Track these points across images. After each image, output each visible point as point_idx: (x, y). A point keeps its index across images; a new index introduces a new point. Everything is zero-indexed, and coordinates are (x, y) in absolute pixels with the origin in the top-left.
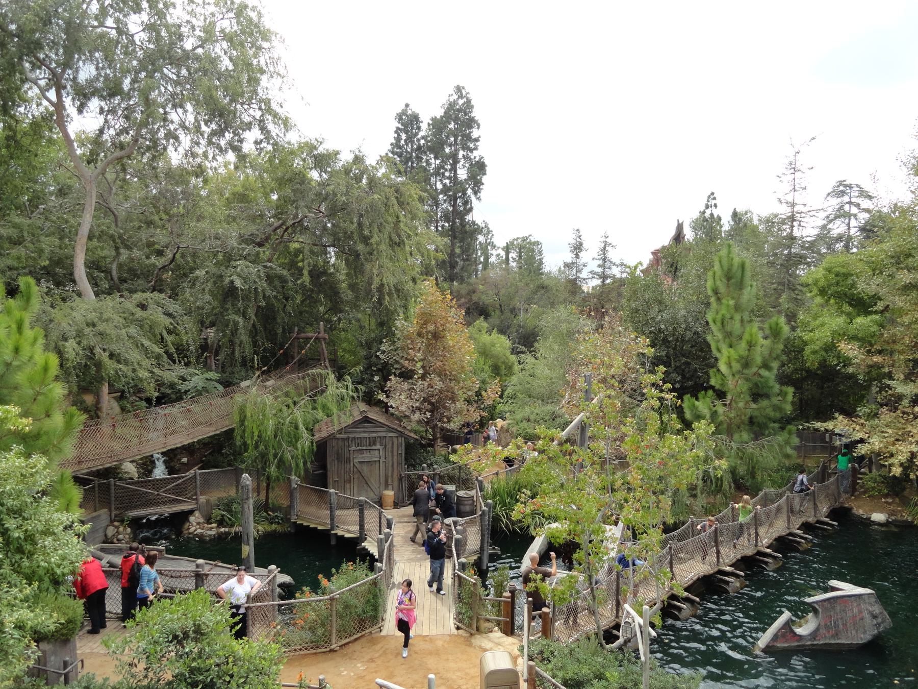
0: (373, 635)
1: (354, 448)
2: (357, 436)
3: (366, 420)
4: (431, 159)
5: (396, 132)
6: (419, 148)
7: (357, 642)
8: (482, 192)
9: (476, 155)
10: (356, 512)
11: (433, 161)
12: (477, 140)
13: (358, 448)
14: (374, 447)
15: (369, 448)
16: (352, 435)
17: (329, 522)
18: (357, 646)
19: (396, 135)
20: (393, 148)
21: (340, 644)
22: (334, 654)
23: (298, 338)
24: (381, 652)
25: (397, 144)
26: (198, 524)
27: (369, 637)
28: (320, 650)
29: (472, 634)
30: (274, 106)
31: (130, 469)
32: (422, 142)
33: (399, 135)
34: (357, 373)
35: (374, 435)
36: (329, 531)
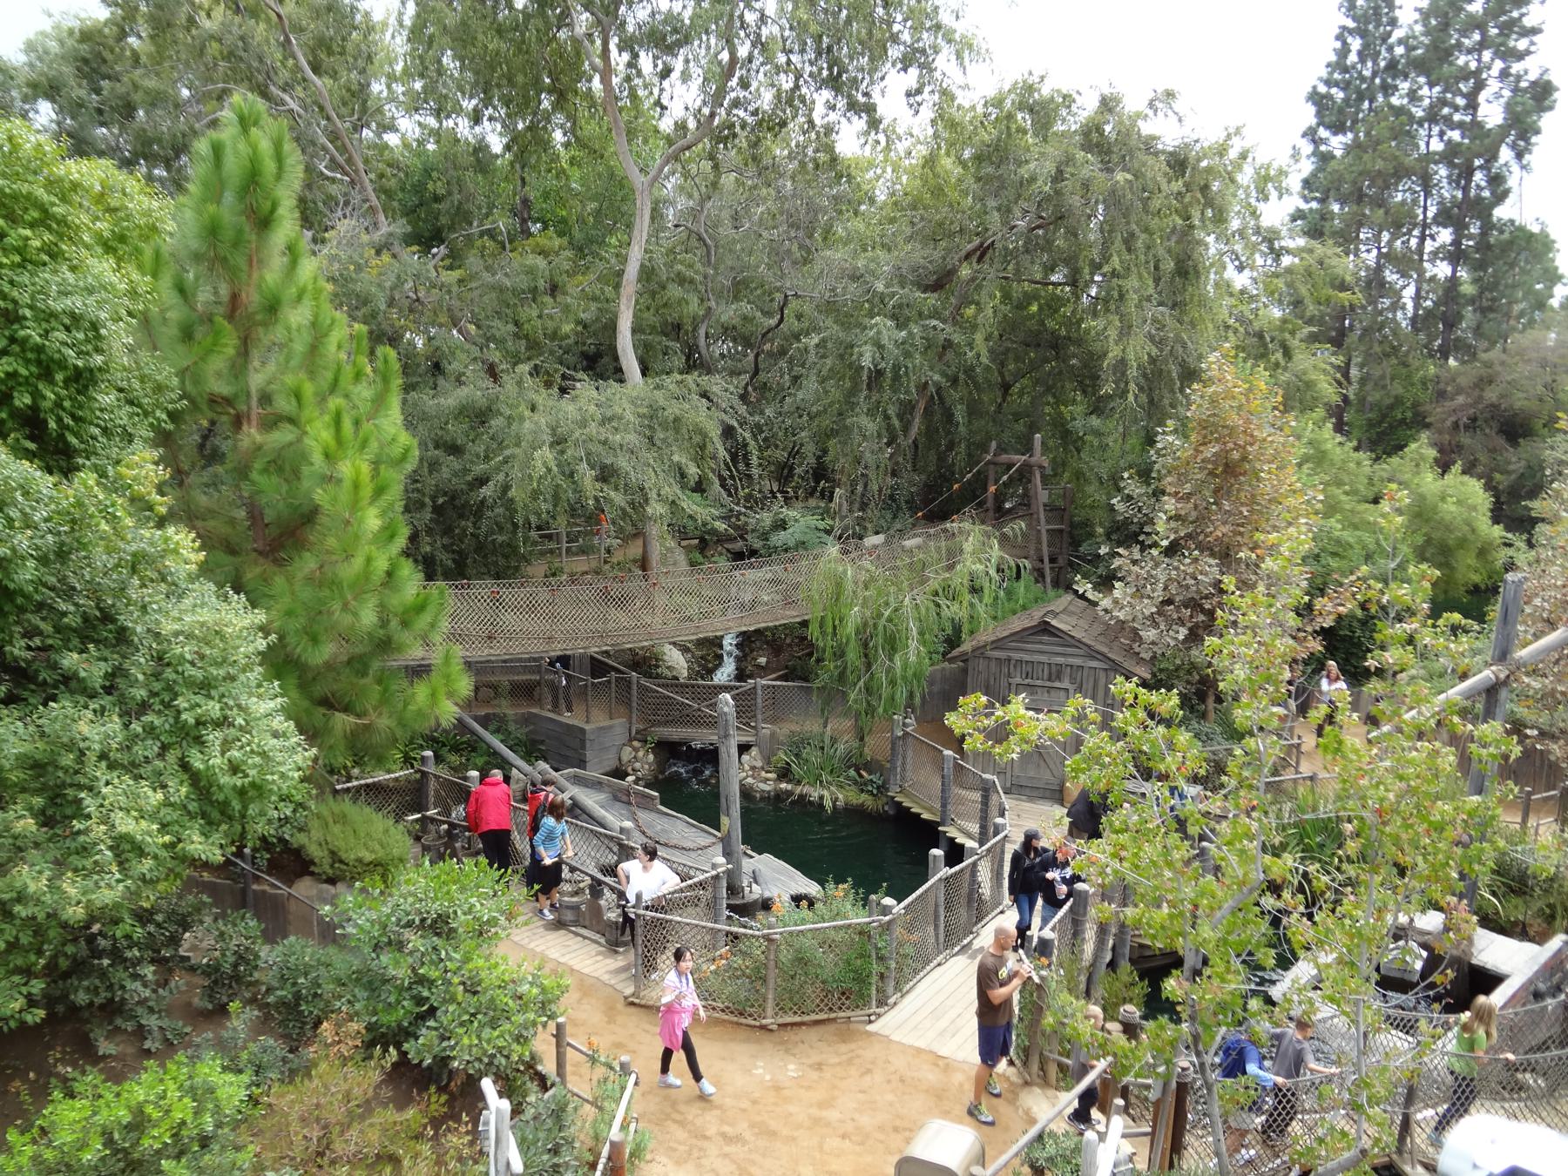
0: (852, 1026)
1: (1018, 680)
2: (1027, 657)
3: (1044, 628)
4: (1420, 88)
5: (1339, 37)
6: (1392, 66)
7: (821, 1029)
8: (1535, 149)
9: (1530, 68)
10: (977, 796)
11: (1425, 91)
12: (1535, 31)
13: (1028, 681)
14: (1057, 684)
15: (1048, 684)
16: (1016, 656)
17: (938, 806)
18: (812, 1034)
19: (1338, 45)
20: (1331, 73)
21: (781, 1021)
22: (765, 1035)
23: (995, 464)
24: (844, 1057)
25: (1340, 65)
26: (753, 768)
27: (844, 1027)
28: (743, 1021)
29: (1027, 1083)
30: (945, 18)
31: (677, 661)
32: (1399, 50)
33: (1345, 43)
34: (1016, 536)
35: (1060, 660)
36: (939, 824)
